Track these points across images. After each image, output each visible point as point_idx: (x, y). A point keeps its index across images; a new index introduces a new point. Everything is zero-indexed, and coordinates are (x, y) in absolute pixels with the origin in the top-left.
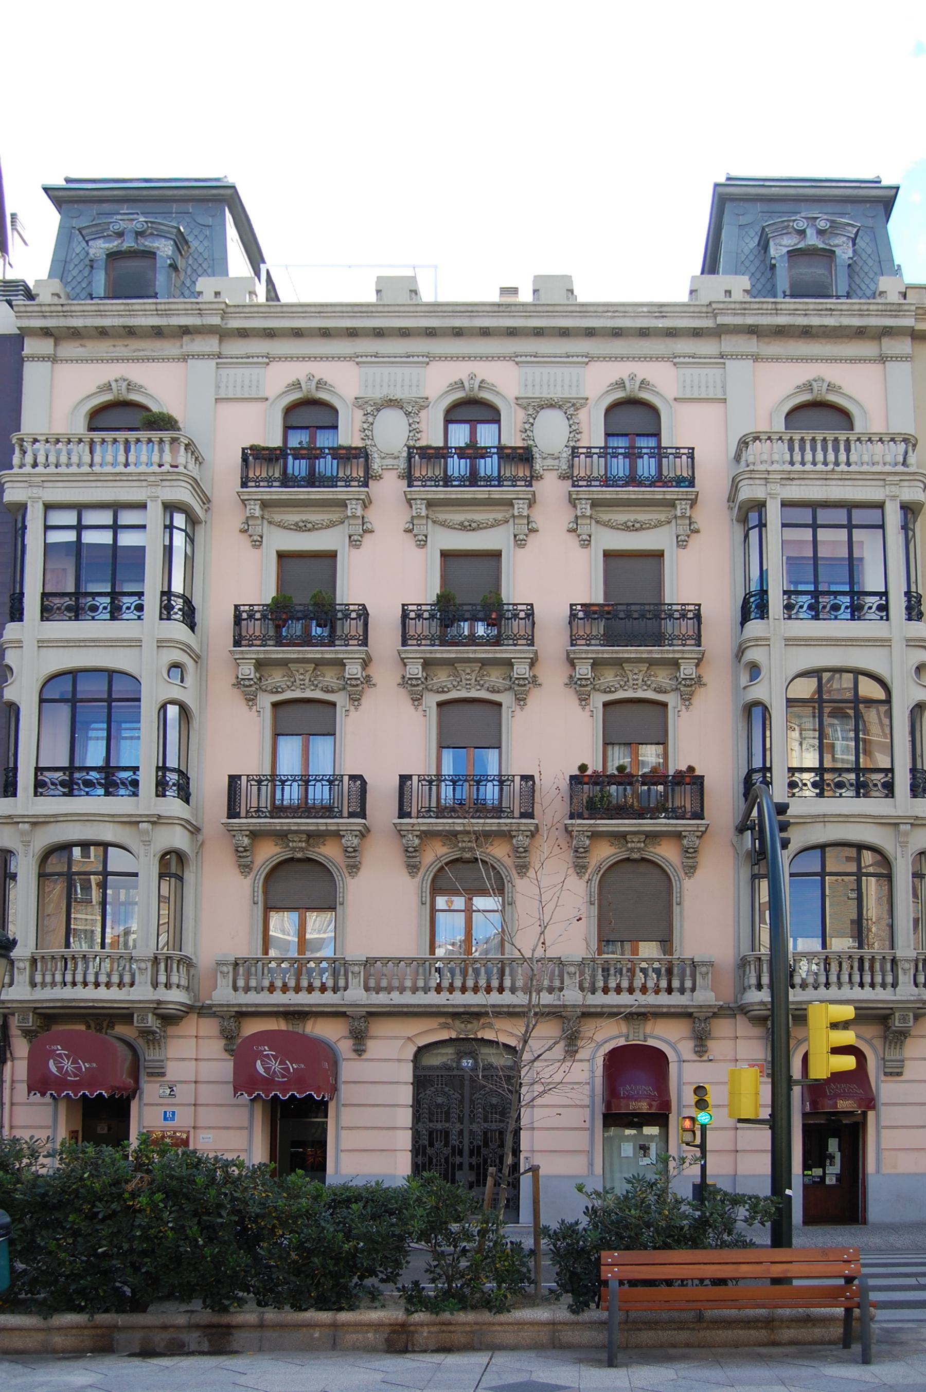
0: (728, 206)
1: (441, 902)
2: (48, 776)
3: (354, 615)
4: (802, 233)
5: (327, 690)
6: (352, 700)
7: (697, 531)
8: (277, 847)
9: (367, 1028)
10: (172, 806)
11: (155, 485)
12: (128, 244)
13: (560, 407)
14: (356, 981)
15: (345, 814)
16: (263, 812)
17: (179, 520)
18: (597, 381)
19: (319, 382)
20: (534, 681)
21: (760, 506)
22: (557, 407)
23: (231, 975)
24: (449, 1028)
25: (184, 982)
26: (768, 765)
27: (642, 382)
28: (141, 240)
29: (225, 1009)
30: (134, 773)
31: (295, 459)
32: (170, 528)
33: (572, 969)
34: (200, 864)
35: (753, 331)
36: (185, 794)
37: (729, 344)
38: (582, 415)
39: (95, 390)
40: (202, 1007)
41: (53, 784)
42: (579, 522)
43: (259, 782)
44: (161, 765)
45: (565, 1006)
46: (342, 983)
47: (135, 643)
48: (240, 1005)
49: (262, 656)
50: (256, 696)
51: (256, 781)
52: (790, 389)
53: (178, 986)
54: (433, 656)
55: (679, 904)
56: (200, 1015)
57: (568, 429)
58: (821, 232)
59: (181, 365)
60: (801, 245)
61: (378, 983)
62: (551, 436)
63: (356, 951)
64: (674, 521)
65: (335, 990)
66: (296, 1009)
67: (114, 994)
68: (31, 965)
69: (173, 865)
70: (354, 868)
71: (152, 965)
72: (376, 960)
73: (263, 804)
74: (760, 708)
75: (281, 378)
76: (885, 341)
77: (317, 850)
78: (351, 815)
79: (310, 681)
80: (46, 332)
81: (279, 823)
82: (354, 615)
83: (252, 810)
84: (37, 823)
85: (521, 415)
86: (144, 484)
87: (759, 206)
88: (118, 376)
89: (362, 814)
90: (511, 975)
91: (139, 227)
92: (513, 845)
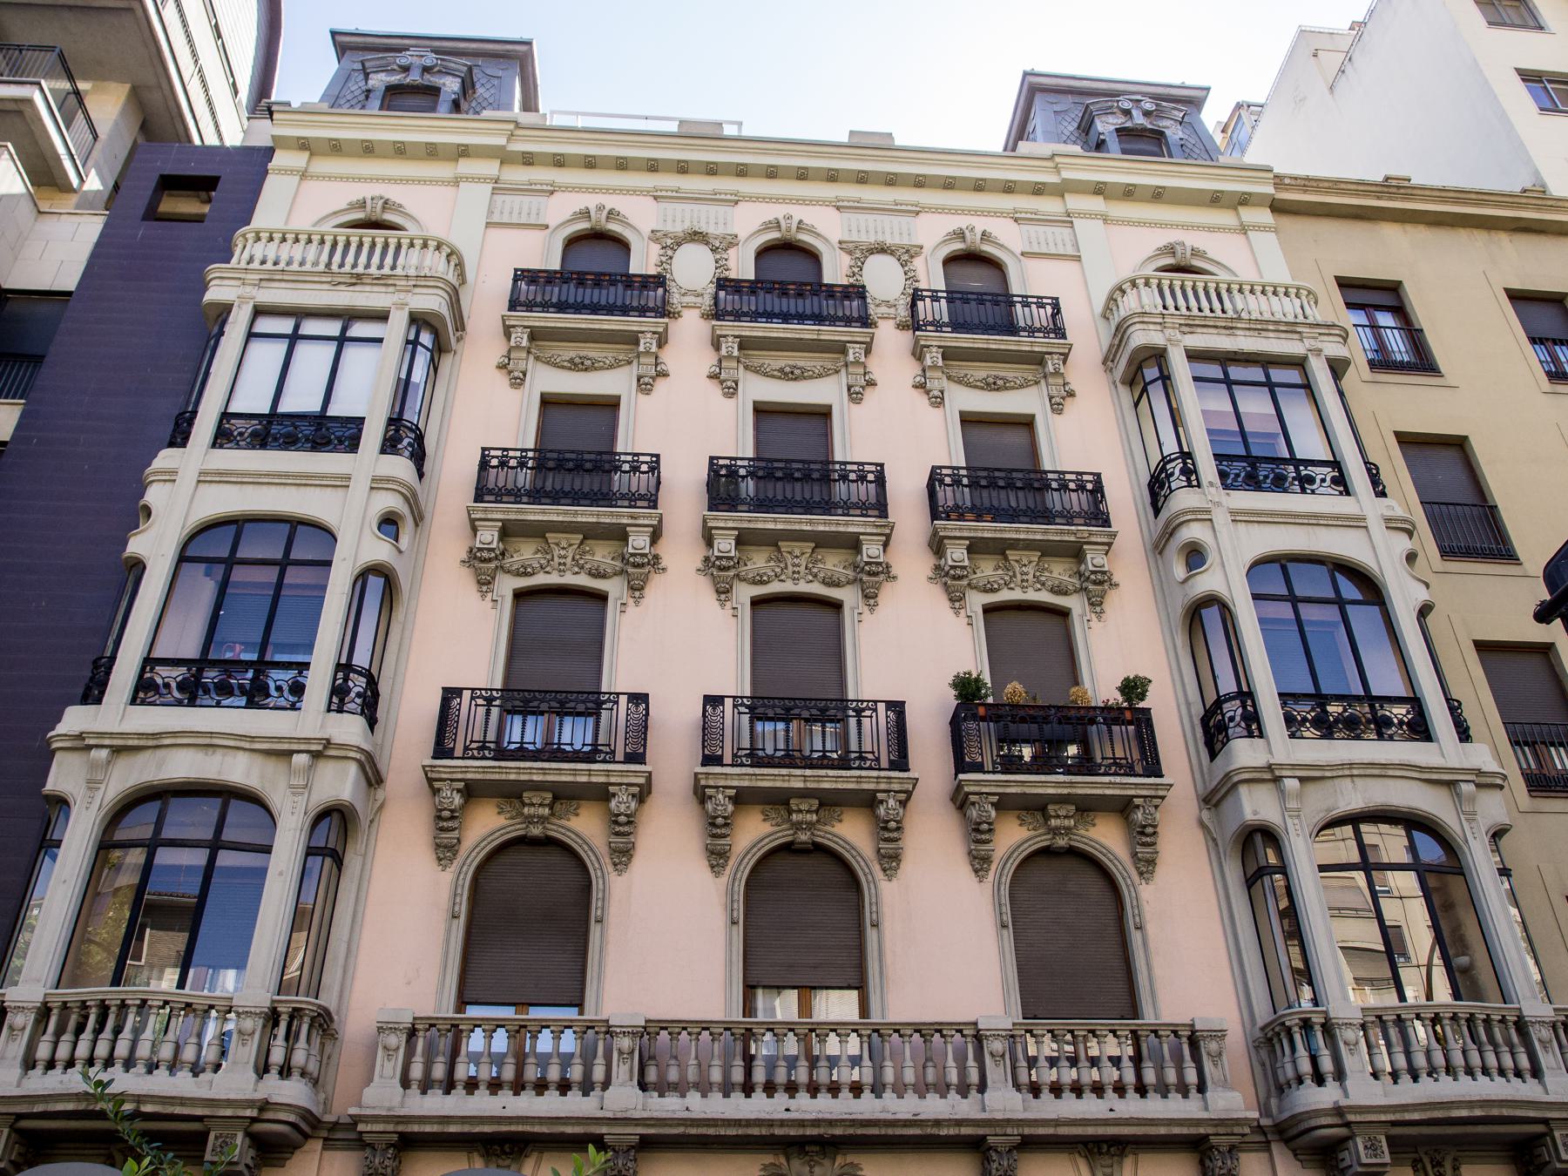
0: (1039, 100)
2: (164, 674)
3: (644, 468)
4: (1127, 113)
5: (597, 574)
7: (665, 374)
10: (349, 729)
12: (414, 77)
13: (892, 253)
14: (389, 1066)
15: (620, 756)
16: (489, 749)
17: (426, 338)
19: (610, 212)
21: (1158, 356)
22: (891, 253)
25: (312, 1067)
26: (1245, 689)
28: (427, 76)
29: (380, 1127)
30: (300, 673)
32: (413, 344)
35: (1099, 190)
37: (1075, 202)
38: (918, 263)
39: (344, 206)
40: (335, 1126)
42: (928, 374)
44: (343, 661)
46: (598, 1073)
47: (342, 482)
51: (485, 699)
52: (756, 226)
53: (303, 1074)
54: (752, 526)
55: (1139, 928)
56: (329, 1144)
58: (1147, 114)
59: (451, 190)
60: (1129, 124)
61: (662, 1075)
62: (884, 282)
64: (843, 371)
65: (587, 1087)
67: (182, 1084)
68: (37, 1022)
69: (334, 833)
70: (623, 855)
71: (264, 1026)
72: (664, 1025)
75: (564, 209)
76: (1242, 210)
80: (304, 145)
81: (513, 771)
83: (474, 745)
84: (1311, 777)
85: (846, 260)
86: (391, 289)
87: (1070, 98)
88: (377, 194)
91: (428, 63)
92: (877, 817)
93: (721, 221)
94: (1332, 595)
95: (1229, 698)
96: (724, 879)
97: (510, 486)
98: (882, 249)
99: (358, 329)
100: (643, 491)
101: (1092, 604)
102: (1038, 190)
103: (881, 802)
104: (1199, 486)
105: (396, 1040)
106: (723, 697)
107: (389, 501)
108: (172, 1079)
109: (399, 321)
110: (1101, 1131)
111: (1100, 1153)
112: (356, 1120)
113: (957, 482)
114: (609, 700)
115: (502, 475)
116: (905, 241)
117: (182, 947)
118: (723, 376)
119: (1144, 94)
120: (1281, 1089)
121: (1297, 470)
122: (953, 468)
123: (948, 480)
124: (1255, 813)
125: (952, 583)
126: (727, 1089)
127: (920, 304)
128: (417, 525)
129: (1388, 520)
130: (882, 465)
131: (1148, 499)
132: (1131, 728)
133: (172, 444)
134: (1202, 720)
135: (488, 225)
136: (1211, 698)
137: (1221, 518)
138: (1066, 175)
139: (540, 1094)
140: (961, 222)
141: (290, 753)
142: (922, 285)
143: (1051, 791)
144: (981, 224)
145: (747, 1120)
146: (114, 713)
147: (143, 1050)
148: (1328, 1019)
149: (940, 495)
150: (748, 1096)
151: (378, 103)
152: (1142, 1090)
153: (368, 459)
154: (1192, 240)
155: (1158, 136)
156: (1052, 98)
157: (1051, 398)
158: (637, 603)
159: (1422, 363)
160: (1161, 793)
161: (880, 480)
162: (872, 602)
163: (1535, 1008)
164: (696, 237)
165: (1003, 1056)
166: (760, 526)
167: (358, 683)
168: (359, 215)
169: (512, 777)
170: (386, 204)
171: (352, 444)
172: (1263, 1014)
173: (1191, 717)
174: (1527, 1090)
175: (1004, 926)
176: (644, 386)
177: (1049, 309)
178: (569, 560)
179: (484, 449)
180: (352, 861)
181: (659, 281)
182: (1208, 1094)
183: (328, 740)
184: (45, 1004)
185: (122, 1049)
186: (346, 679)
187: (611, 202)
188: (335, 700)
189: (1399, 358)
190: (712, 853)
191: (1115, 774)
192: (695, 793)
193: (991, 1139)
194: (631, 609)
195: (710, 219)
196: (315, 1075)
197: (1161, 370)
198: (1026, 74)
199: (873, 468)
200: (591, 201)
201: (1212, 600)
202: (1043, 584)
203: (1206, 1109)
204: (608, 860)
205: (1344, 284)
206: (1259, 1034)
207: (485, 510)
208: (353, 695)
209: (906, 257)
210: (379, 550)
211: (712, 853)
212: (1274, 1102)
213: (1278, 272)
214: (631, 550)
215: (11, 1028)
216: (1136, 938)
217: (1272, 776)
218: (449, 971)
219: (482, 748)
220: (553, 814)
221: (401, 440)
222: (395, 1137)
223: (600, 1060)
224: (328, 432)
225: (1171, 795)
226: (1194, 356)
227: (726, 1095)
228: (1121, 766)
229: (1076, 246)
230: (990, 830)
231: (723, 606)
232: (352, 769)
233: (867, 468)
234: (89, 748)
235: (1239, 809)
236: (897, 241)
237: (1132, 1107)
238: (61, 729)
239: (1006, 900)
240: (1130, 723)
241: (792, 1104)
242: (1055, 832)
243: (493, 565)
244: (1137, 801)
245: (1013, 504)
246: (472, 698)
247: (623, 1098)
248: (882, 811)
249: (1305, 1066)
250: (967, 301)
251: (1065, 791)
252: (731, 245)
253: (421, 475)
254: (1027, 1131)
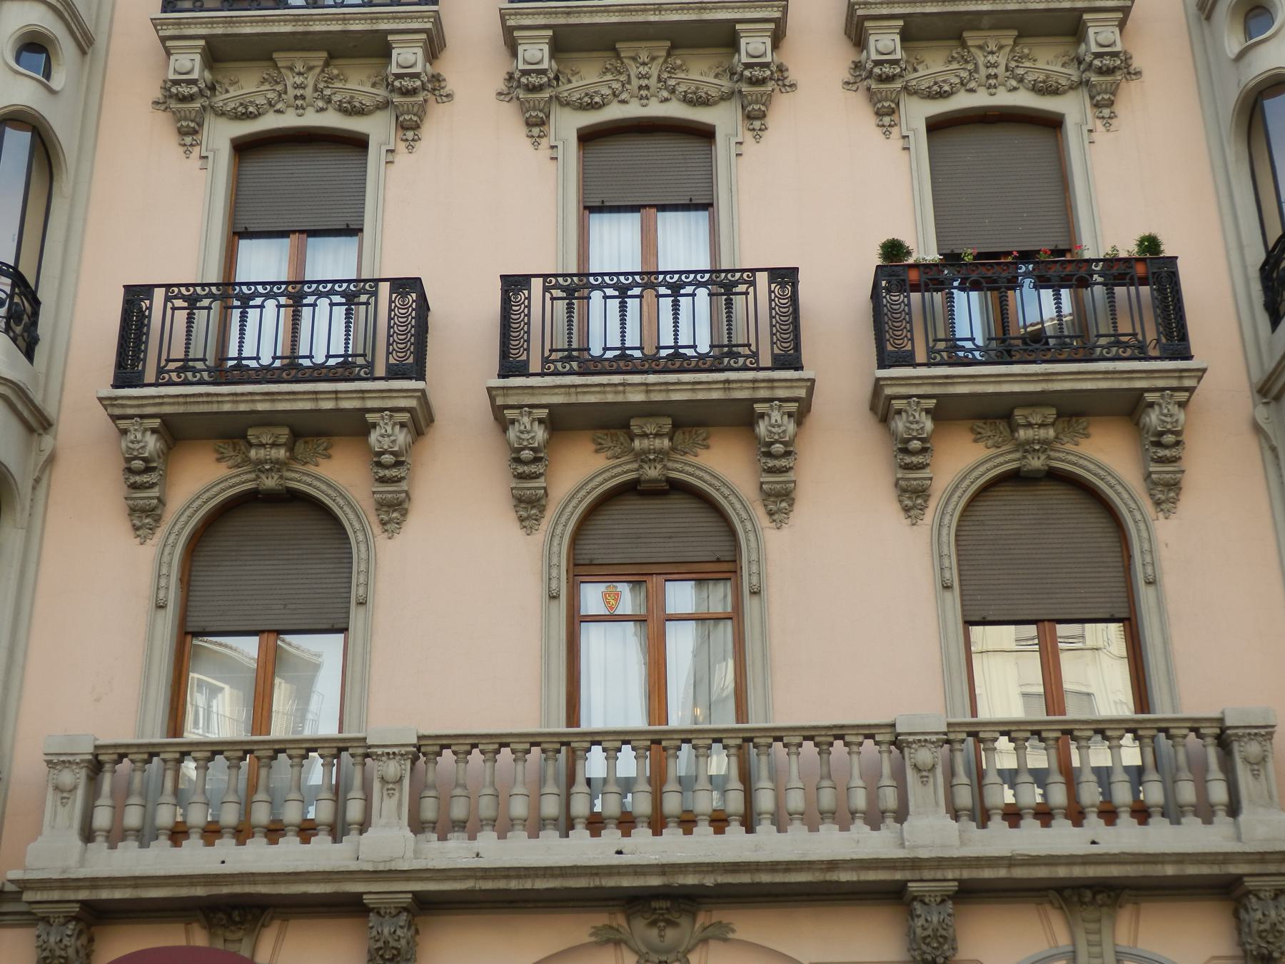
1: (593, 597)
5: (352, 110)
6: (403, 127)
8: (223, 465)
9: (412, 944)
14: (390, 804)
15: (380, 370)
20: (779, 77)
23: (80, 793)
24: (617, 943)
29: (56, 895)
33: (924, 756)
34: (39, 508)
43: (192, 302)
45: (915, 864)
46: (354, 811)
48: (94, 883)
49: (219, 30)
50: (201, 125)
54: (573, 20)
63: (394, 720)
65: (337, 830)
66: (237, 889)
70: (394, 510)
72: (444, 743)
73: (197, 352)
77: (311, 468)
78: (395, 372)
79: (316, 89)
83: (172, 366)
90: (773, 777)
92: (757, 438)
96: (540, 536)
101: (1097, 105)
103: (762, 416)
105: (74, 778)
106: (527, 278)
110: (1077, 872)
111: (1082, 903)
112: (25, 885)
117: (980, 628)
125: (879, 88)
126: (536, 826)
132: (1145, 290)
134: (1262, 269)
139: (274, 842)
143: (1017, 388)
145: (758, 863)
152: (749, 823)
158: (410, 148)
160: (1187, 383)
162: (757, 124)
166: (318, 27)
169: (227, 407)
173: (1245, 267)
175: (554, 597)
178: (1001, 70)
182: (1242, 818)
190: (904, 490)
192: (873, 408)
193: (913, 886)
194: (402, 157)
202: (1021, 80)
203: (1239, 838)
204: (373, 519)
207: (178, 23)
211: (904, 490)
214: (745, 59)
219: (184, 369)
220: (293, 458)
222: (76, 908)
223: (356, 793)
225: (1206, 388)
227: (657, 832)
228: (1126, 346)
230: (1178, 443)
231: (536, 145)
237: (1126, 837)
240: (1143, 281)
241: (626, 843)
242: (1026, 448)
243: (196, 105)
244: (1150, 397)
247: (388, 843)
248: (762, 428)
251: (1038, 387)
254: (966, 874)
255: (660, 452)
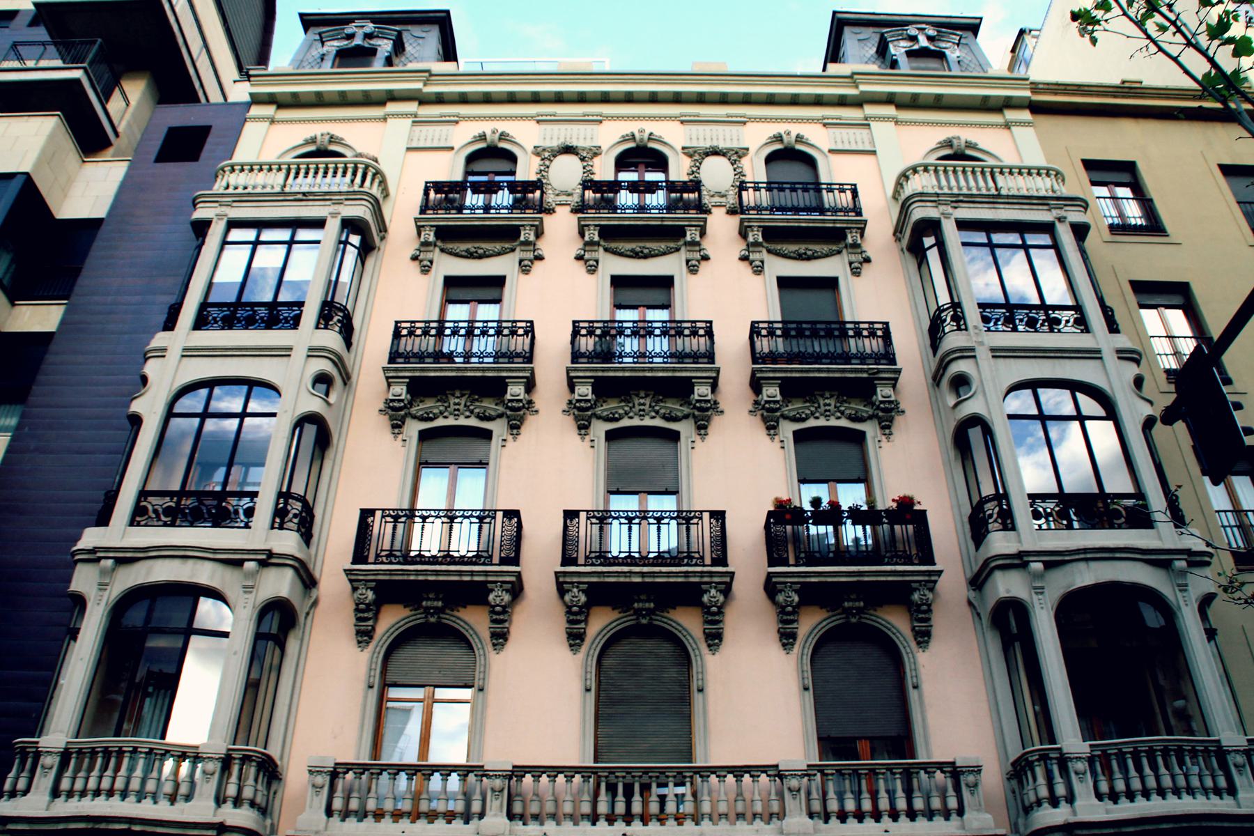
0: (848, 31)
3: (521, 332)
10: (287, 542)
11: (339, 203)
12: (358, 41)
13: (724, 155)
15: (496, 560)
16: (396, 556)
17: (355, 239)
18: (756, 135)
19: (502, 134)
23: (326, 789)
25: (259, 799)
27: (798, 136)
31: (474, 193)
35: (889, 100)
36: (307, 535)
37: (870, 110)
38: (745, 163)
39: (301, 142)
41: (155, 511)
44: (284, 489)
47: (284, 352)
55: (915, 687)
57: (733, 173)
59: (380, 125)
60: (916, 47)
62: (716, 175)
69: (278, 625)
74: (978, 429)
75: (468, 130)
77: (456, 613)
82: (521, 332)
83: (383, 553)
84: (1055, 561)
87: (871, 30)
88: (325, 131)
89: (515, 561)
93: (589, 136)
94: (1035, 412)
95: (988, 499)
97: (416, 350)
98: (715, 152)
99: (303, 234)
100: (519, 350)
102: (842, 102)
104: (966, 329)
105: (323, 780)
107: (325, 366)
108: (155, 806)
109: (333, 226)
113: (771, 333)
114: (488, 516)
115: (410, 341)
116: (735, 145)
118: (586, 257)
119: (927, 23)
120: (1027, 810)
121: (1047, 315)
122: (769, 322)
123: (764, 332)
124: (1008, 591)
127: (744, 194)
128: (345, 384)
129: (1119, 351)
130: (711, 322)
131: (928, 342)
133: (164, 330)
135: (408, 149)
136: (976, 499)
137: (983, 354)
138: (863, 88)
140: (780, 128)
141: (243, 561)
142: (747, 179)
144: (795, 129)
146: (118, 533)
147: (135, 785)
148: (1062, 754)
149: (758, 344)
150: (594, 824)
151: (330, 63)
153: (308, 334)
154: (966, 135)
155: (940, 56)
156: (857, 29)
157: (851, 264)
158: (515, 439)
159: (1153, 226)
160: (933, 578)
161: (709, 333)
163: (1230, 736)
164: (568, 150)
165: (799, 790)
167: (296, 506)
168: (312, 148)
169: (412, 578)
170: (333, 139)
171: (295, 323)
172: (1015, 752)
174: (1223, 805)
176: (525, 268)
177: (849, 194)
179: (397, 322)
180: (292, 645)
181: (537, 185)
182: (965, 817)
183: (270, 551)
184: (66, 749)
185: (119, 784)
186: (286, 503)
187: (502, 126)
188: (278, 520)
189: (1133, 222)
191: (688, 565)
194: (510, 443)
195: (579, 136)
196: (264, 805)
197: (937, 239)
198: (834, 13)
199: (703, 325)
200: (487, 127)
201: (976, 420)
205: (1089, 165)
206: (1010, 768)
208: (290, 515)
209: (735, 157)
210: (314, 404)
212: (1021, 821)
213: (1036, 158)
215: (43, 767)
216: (913, 695)
217: (1019, 561)
218: (366, 727)
221: (331, 318)
224: (280, 314)
226: (962, 225)
229: (872, 142)
232: (289, 574)
233: (699, 325)
234: (98, 560)
235: (996, 588)
236: (728, 145)
238: (81, 545)
239: (808, 667)
244: (914, 585)
245: (817, 349)
246: (383, 517)
249: (1043, 792)
250: (782, 190)
252: (596, 154)
253: (349, 344)
255: (858, 609)
